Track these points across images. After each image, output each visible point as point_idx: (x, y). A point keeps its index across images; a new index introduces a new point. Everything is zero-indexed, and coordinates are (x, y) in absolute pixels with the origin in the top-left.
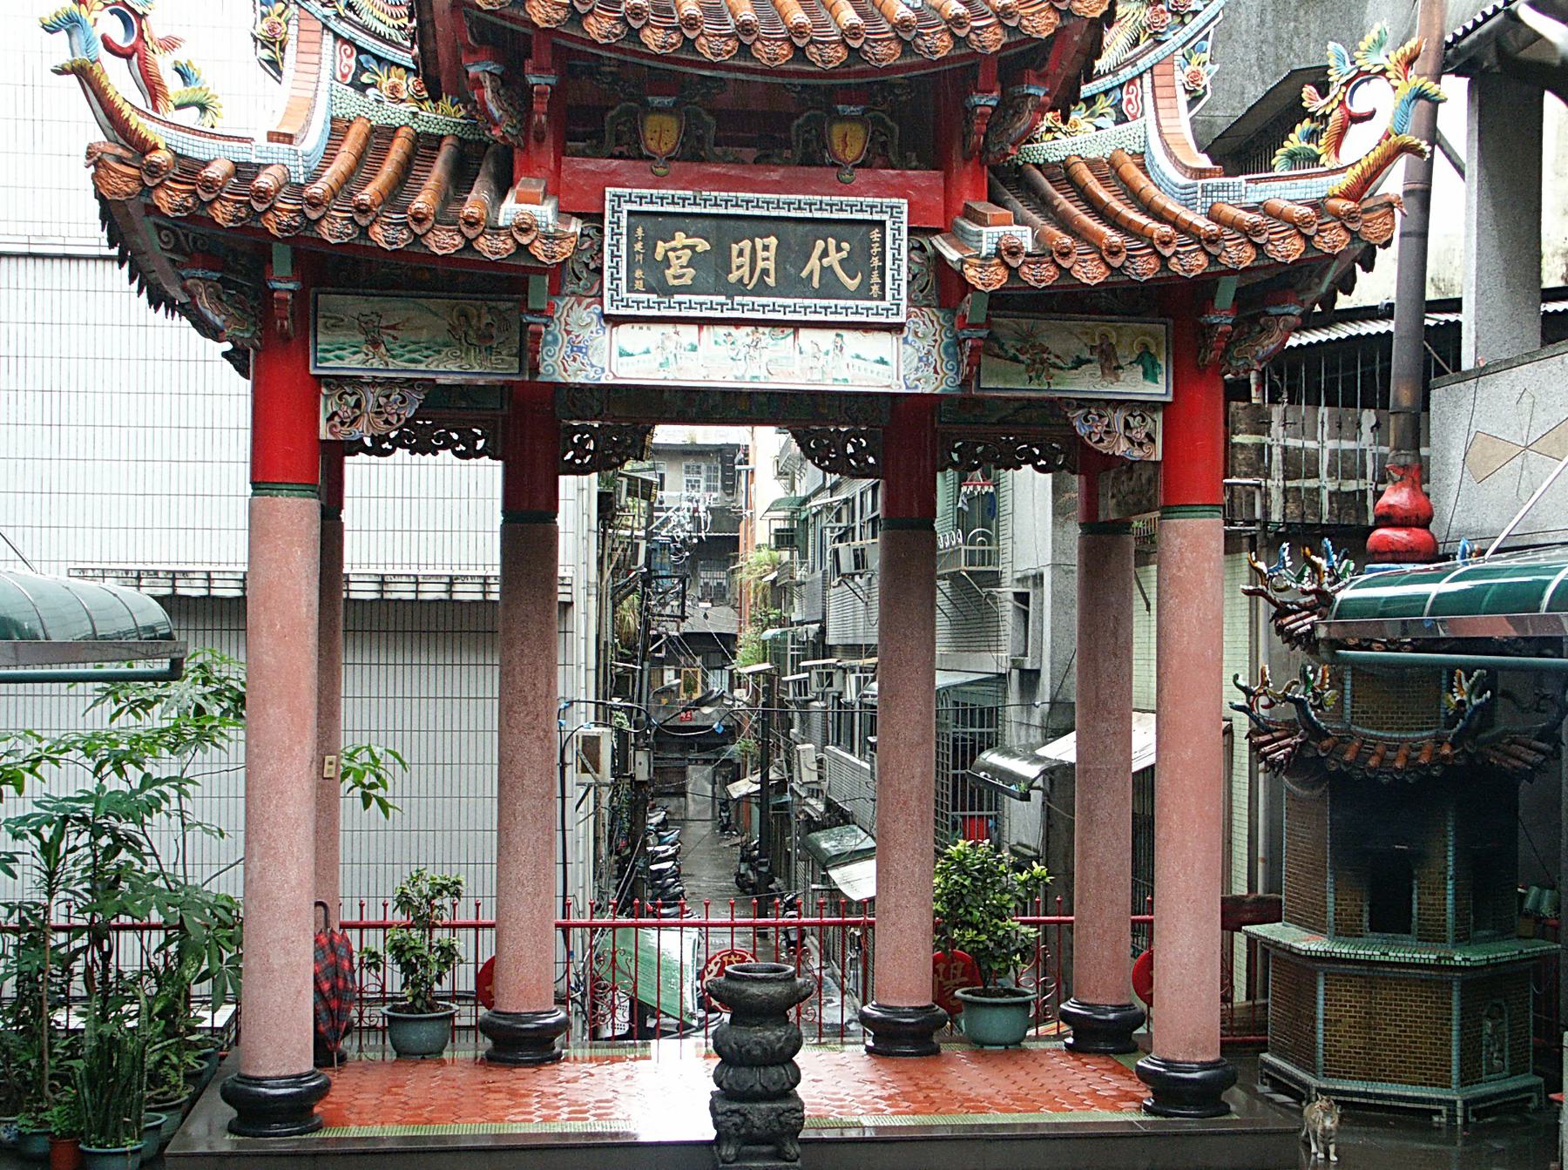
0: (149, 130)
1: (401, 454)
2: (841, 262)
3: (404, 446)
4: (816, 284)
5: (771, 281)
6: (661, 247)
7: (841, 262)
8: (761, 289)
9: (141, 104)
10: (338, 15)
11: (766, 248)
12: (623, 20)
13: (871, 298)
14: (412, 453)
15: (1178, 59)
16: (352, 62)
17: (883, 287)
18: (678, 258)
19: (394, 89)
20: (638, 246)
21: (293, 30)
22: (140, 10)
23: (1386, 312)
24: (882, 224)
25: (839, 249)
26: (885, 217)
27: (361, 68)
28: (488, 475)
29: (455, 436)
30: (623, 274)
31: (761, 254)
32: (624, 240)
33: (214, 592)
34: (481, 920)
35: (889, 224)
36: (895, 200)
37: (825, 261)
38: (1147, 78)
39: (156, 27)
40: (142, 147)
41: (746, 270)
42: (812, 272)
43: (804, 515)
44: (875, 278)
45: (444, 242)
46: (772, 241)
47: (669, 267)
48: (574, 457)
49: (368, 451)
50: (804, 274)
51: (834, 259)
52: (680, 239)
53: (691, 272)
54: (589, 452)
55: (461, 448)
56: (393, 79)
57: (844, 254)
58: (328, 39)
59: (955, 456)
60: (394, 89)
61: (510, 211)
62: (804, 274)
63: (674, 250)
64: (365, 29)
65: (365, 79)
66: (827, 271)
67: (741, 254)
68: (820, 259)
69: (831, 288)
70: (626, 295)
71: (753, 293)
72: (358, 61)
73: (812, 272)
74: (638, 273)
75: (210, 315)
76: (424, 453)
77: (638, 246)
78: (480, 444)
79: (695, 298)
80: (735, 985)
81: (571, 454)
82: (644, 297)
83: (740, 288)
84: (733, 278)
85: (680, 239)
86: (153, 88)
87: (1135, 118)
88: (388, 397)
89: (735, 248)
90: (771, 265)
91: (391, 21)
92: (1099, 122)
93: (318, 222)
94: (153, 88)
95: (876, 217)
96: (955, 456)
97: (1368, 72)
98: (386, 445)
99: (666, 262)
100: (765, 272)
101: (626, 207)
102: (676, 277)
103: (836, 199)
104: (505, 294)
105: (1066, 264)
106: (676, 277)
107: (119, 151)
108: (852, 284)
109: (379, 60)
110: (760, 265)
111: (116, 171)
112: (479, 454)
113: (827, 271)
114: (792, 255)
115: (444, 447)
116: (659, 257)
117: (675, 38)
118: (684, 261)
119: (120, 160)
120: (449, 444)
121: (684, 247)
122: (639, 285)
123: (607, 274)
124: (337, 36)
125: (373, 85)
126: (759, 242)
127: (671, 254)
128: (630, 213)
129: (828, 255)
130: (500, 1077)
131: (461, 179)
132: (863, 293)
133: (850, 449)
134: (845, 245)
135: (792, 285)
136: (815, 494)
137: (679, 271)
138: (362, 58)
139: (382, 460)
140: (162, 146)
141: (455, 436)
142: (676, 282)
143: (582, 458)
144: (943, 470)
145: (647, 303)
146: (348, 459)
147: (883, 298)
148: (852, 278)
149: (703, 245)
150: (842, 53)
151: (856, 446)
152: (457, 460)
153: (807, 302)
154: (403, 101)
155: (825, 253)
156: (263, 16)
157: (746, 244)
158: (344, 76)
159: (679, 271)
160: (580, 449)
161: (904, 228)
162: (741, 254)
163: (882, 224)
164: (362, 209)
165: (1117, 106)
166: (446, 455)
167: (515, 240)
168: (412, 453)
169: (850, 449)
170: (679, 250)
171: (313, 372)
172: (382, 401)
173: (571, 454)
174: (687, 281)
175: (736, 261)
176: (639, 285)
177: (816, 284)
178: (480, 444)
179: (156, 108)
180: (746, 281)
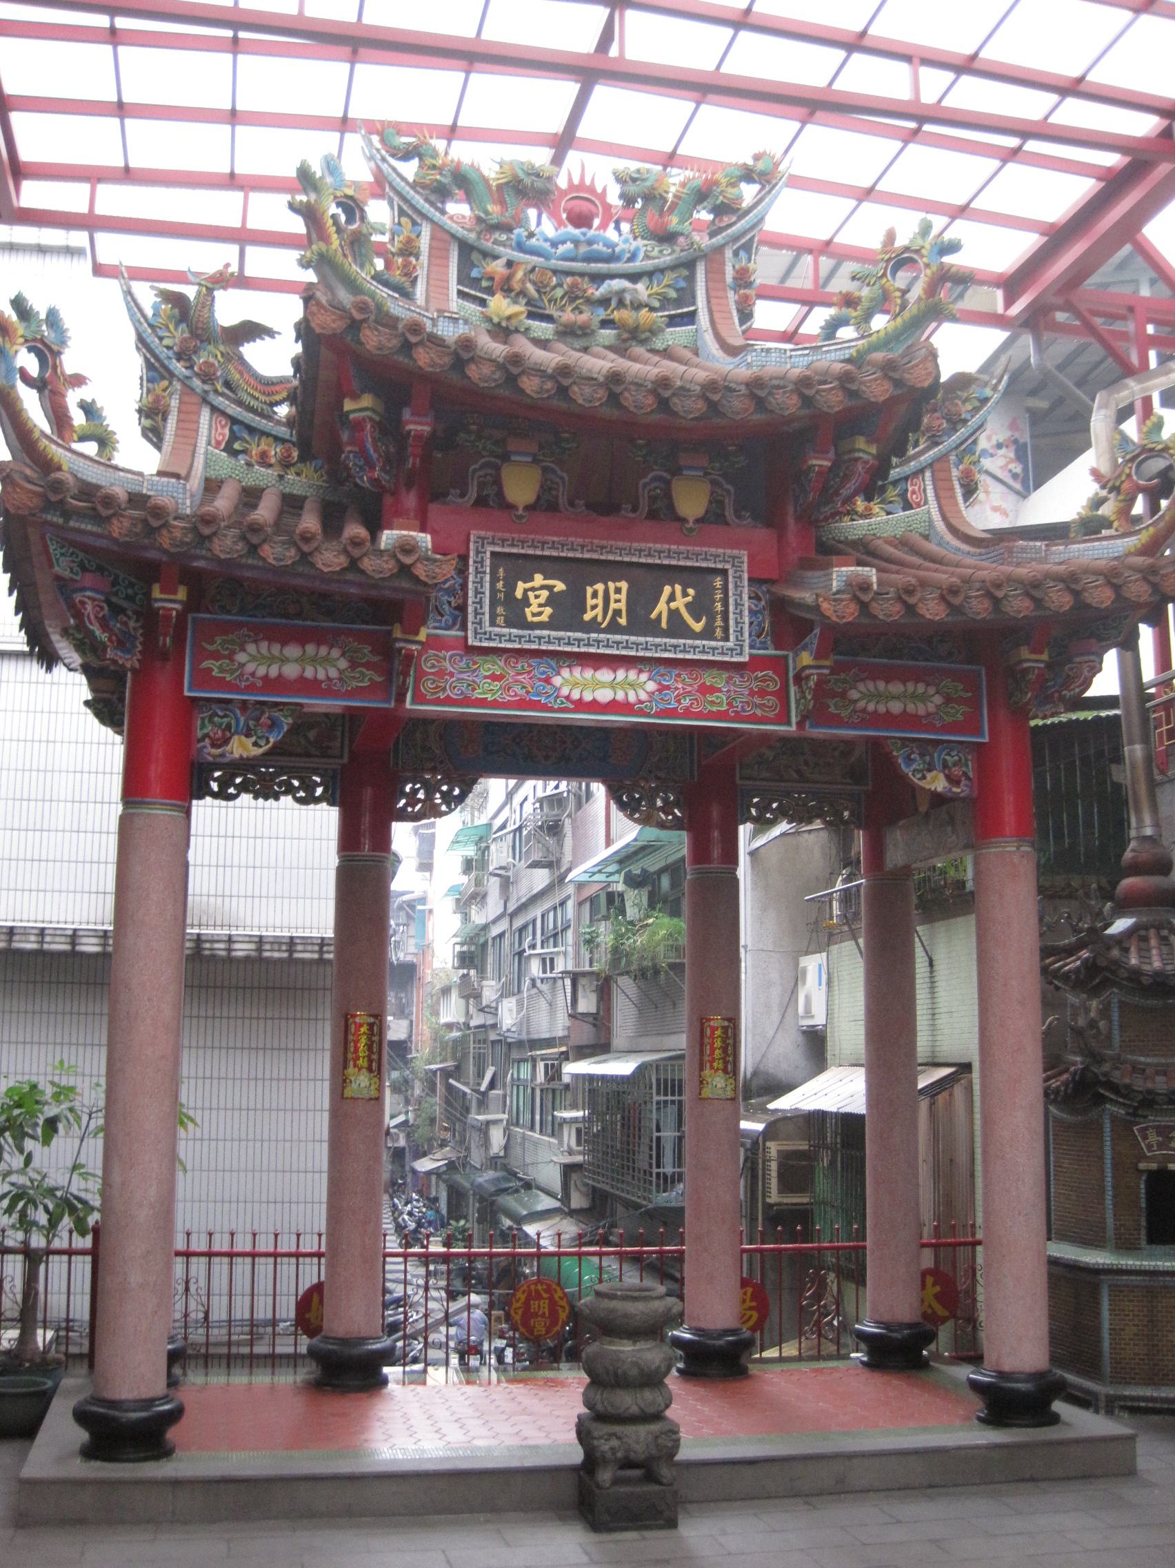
0: (56, 452)
1: (246, 798)
2: (687, 606)
3: (247, 791)
4: (664, 625)
5: (623, 621)
6: (521, 586)
7: (687, 606)
8: (614, 628)
9: (48, 430)
10: (216, 391)
11: (618, 591)
12: (345, 551)
13: (715, 639)
14: (256, 798)
15: (953, 458)
16: (227, 431)
17: (726, 629)
18: (537, 597)
19: (264, 455)
20: (500, 585)
21: (174, 403)
22: (55, 348)
23: (1109, 702)
24: (724, 572)
25: (685, 594)
26: (727, 566)
27: (234, 437)
28: (325, 819)
29: (296, 783)
30: (487, 609)
31: (613, 596)
32: (488, 578)
33: (46, 946)
34: (302, 1250)
35: (731, 572)
36: (736, 552)
37: (673, 605)
38: (928, 474)
39: (70, 363)
40: (46, 465)
41: (599, 610)
42: (660, 615)
43: (482, 940)
44: (719, 623)
45: (330, 559)
46: (624, 585)
47: (529, 605)
48: (406, 805)
49: (215, 796)
50: (653, 616)
51: (680, 603)
52: (539, 579)
53: (548, 611)
54: (420, 800)
55: (302, 794)
56: (263, 447)
57: (689, 599)
58: (205, 414)
59: (753, 811)
60: (264, 455)
61: (388, 537)
62: (653, 616)
63: (533, 589)
64: (240, 403)
65: (237, 446)
66: (674, 614)
67: (595, 595)
68: (668, 602)
69: (677, 627)
70: (489, 629)
71: (605, 631)
72: (231, 431)
73: (660, 615)
74: (500, 610)
75: (98, 633)
76: (266, 799)
77: (500, 585)
78: (319, 791)
79: (554, 634)
80: (606, 1304)
81: (403, 802)
82: (506, 631)
83: (593, 626)
84: (587, 617)
85: (539, 579)
86: (59, 417)
87: (919, 505)
88: (258, 719)
89: (589, 590)
90: (622, 606)
91: (263, 398)
92: (889, 507)
93: (209, 538)
94: (59, 417)
95: (719, 566)
96: (753, 811)
97: (1152, 450)
98: (232, 790)
99: (526, 602)
100: (617, 612)
101: (490, 549)
102: (534, 615)
103: (682, 548)
104: (382, 617)
105: (912, 601)
106: (534, 615)
107: (28, 472)
108: (698, 627)
109: (251, 430)
110: (613, 606)
111: (22, 488)
112: (317, 800)
113: (674, 614)
114: (641, 602)
115: (286, 793)
116: (519, 594)
117: (549, 385)
118: (542, 600)
119: (28, 479)
120: (290, 790)
121: (543, 587)
122: (500, 620)
123: (470, 609)
124: (214, 409)
125: (244, 452)
126: (611, 585)
127: (531, 594)
128: (493, 553)
129: (673, 600)
130: (333, 1404)
131: (332, 520)
132: (708, 633)
133: (659, 803)
134: (691, 591)
135: (640, 622)
136: (495, 921)
137: (538, 609)
138: (235, 428)
139: (231, 803)
140: (65, 467)
141: (296, 783)
142: (536, 619)
143: (413, 806)
144: (744, 822)
145: (507, 637)
146: (194, 802)
147: (726, 639)
148: (698, 621)
149: (560, 586)
150: (701, 405)
151: (665, 800)
152: (297, 806)
153: (658, 640)
154: (270, 466)
155: (672, 598)
156: (149, 391)
157: (600, 587)
158: (218, 443)
159: (538, 609)
160: (412, 801)
161: (746, 576)
162: (595, 595)
163: (724, 572)
164: (255, 528)
165: (903, 496)
166: (287, 800)
167: (398, 561)
168: (256, 798)
169: (659, 803)
170: (537, 593)
171: (186, 693)
172: (251, 723)
173: (403, 802)
174: (544, 618)
175: (590, 602)
176: (500, 620)
177: (664, 625)
178: (319, 791)
179: (61, 436)
180: (600, 619)
